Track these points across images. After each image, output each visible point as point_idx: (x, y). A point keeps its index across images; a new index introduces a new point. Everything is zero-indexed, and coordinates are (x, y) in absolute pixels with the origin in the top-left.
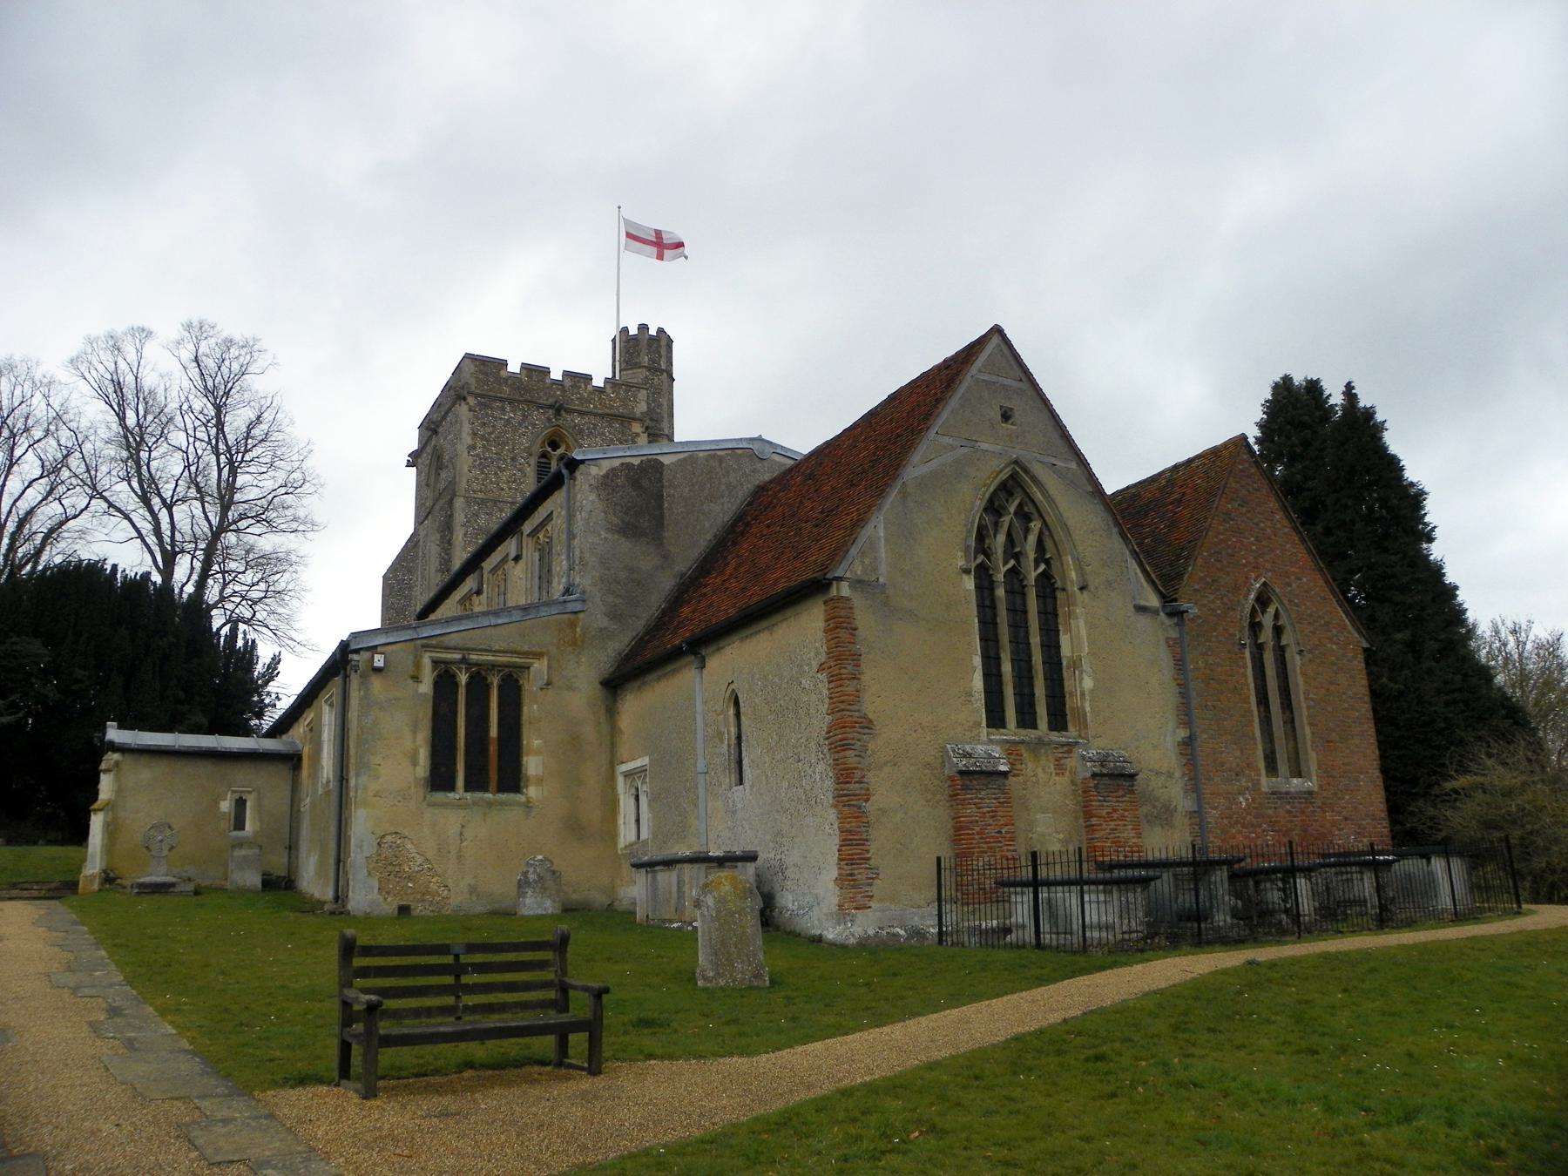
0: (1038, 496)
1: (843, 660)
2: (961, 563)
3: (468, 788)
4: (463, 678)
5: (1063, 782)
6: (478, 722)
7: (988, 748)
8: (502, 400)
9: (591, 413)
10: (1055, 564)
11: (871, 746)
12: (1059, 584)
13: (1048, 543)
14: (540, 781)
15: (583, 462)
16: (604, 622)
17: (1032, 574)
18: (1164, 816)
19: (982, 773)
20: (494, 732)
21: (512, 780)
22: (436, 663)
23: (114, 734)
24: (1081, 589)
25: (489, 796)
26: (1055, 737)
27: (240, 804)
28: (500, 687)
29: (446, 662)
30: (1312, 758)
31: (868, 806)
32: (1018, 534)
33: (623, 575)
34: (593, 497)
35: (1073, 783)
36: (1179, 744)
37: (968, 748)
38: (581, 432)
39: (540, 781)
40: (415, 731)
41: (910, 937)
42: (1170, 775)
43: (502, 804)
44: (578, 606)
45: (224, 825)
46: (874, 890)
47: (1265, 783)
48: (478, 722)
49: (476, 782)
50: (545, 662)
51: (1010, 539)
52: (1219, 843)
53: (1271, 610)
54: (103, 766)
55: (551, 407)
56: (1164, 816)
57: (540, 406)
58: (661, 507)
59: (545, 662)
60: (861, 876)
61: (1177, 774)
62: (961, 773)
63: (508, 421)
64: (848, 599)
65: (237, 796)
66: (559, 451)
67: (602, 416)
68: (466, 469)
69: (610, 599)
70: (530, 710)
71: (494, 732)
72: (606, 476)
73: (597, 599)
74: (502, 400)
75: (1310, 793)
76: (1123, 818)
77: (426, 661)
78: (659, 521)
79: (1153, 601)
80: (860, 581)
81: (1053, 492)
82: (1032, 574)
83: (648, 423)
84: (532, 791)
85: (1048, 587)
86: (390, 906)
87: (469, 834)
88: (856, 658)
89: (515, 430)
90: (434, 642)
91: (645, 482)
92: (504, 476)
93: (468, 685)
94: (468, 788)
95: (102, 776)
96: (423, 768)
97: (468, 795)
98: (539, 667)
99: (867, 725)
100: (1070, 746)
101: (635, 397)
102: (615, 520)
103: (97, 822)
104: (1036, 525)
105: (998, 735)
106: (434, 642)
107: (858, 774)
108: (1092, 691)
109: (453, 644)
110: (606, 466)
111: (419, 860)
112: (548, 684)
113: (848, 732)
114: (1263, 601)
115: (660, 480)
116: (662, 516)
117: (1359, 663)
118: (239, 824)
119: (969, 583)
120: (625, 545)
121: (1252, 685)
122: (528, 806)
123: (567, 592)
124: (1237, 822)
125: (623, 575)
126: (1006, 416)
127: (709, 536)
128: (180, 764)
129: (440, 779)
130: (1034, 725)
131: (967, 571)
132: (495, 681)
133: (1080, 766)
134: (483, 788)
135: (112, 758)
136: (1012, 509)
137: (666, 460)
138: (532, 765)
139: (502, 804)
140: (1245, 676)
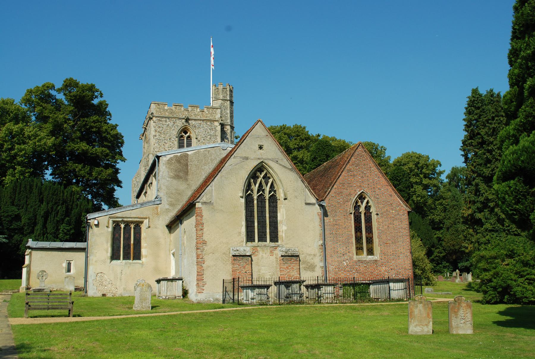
0: (271, 171)
1: (199, 225)
2: (241, 194)
3: (124, 259)
4: (122, 226)
5: (273, 258)
6: (127, 239)
7: (246, 248)
8: (165, 117)
9: (198, 120)
10: (277, 192)
11: (205, 249)
12: (278, 198)
13: (275, 185)
14: (146, 256)
15: (161, 156)
16: (167, 207)
17: (267, 196)
18: (311, 268)
19: (240, 256)
20: (132, 242)
21: (137, 256)
22: (114, 222)
23: (31, 243)
24: (285, 199)
25: (131, 261)
26: (273, 244)
27: (69, 264)
28: (134, 228)
29: (117, 222)
30: (377, 248)
31: (204, 265)
32: (264, 184)
33: (174, 191)
34: (164, 167)
35: (276, 258)
36: (319, 246)
37: (238, 249)
38: (195, 127)
39: (146, 256)
40: (107, 243)
41: (214, 301)
42: (315, 255)
43: (135, 263)
44: (159, 202)
45: (64, 271)
46: (204, 288)
47: (355, 258)
48: (127, 239)
49: (127, 257)
50: (148, 220)
51: (261, 185)
52: (333, 276)
53: (365, 201)
54: (26, 254)
55: (183, 119)
56: (311, 268)
57: (180, 119)
58: (187, 169)
59: (148, 220)
60: (201, 284)
61: (318, 255)
62: (233, 256)
63: (168, 125)
64: (200, 208)
65: (68, 262)
66: (187, 135)
67: (203, 120)
68: (153, 144)
69: (170, 199)
70: (143, 235)
71: (132, 242)
72: (169, 160)
73: (165, 200)
74: (165, 117)
75: (376, 261)
76: (293, 268)
77: (111, 222)
78: (187, 173)
79: (313, 200)
80: (205, 203)
81: (276, 170)
82: (267, 196)
83: (220, 122)
84: (143, 259)
85: (273, 200)
86: (99, 294)
87: (124, 272)
88: (202, 224)
89: (170, 128)
90: (113, 215)
91: (182, 161)
92: (167, 146)
93: (124, 228)
94: (124, 259)
95: (26, 257)
96: (109, 254)
97: (124, 261)
98: (146, 221)
99: (205, 243)
100: (276, 248)
101: (216, 112)
102: (172, 174)
103: (24, 271)
104: (270, 181)
105: (249, 244)
106: (113, 215)
107: (201, 256)
108: (286, 230)
109: (119, 216)
110: (168, 157)
111: (108, 280)
112: (149, 227)
113: (200, 244)
114: (361, 197)
115: (187, 160)
116: (188, 172)
117: (406, 216)
118: (69, 270)
119: (243, 201)
120: (175, 182)
121: (353, 226)
122: (142, 264)
123: (156, 198)
124: (342, 270)
125: (174, 191)
126: (261, 148)
127: (204, 177)
128: (49, 253)
129: (115, 256)
130: (254, 241)
131: (242, 197)
132: (132, 226)
133: (279, 253)
134: (129, 259)
135: (28, 251)
136: (262, 176)
137: (189, 153)
138: (144, 251)
139: (135, 263)
140: (350, 223)
